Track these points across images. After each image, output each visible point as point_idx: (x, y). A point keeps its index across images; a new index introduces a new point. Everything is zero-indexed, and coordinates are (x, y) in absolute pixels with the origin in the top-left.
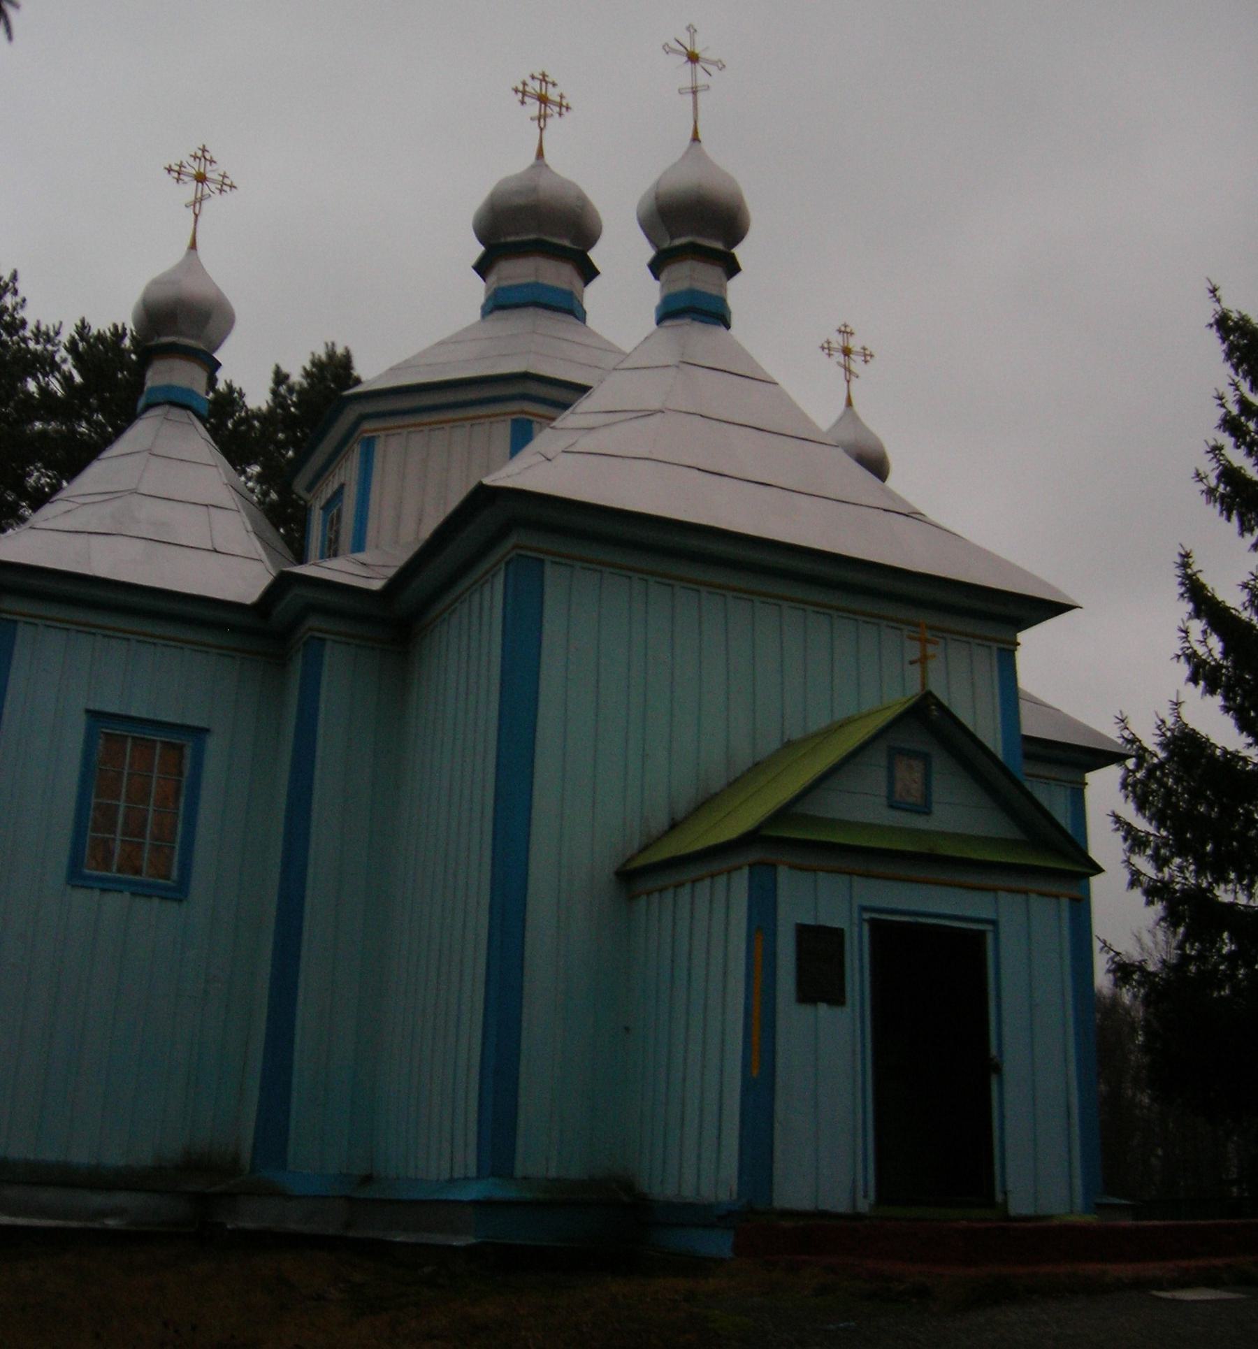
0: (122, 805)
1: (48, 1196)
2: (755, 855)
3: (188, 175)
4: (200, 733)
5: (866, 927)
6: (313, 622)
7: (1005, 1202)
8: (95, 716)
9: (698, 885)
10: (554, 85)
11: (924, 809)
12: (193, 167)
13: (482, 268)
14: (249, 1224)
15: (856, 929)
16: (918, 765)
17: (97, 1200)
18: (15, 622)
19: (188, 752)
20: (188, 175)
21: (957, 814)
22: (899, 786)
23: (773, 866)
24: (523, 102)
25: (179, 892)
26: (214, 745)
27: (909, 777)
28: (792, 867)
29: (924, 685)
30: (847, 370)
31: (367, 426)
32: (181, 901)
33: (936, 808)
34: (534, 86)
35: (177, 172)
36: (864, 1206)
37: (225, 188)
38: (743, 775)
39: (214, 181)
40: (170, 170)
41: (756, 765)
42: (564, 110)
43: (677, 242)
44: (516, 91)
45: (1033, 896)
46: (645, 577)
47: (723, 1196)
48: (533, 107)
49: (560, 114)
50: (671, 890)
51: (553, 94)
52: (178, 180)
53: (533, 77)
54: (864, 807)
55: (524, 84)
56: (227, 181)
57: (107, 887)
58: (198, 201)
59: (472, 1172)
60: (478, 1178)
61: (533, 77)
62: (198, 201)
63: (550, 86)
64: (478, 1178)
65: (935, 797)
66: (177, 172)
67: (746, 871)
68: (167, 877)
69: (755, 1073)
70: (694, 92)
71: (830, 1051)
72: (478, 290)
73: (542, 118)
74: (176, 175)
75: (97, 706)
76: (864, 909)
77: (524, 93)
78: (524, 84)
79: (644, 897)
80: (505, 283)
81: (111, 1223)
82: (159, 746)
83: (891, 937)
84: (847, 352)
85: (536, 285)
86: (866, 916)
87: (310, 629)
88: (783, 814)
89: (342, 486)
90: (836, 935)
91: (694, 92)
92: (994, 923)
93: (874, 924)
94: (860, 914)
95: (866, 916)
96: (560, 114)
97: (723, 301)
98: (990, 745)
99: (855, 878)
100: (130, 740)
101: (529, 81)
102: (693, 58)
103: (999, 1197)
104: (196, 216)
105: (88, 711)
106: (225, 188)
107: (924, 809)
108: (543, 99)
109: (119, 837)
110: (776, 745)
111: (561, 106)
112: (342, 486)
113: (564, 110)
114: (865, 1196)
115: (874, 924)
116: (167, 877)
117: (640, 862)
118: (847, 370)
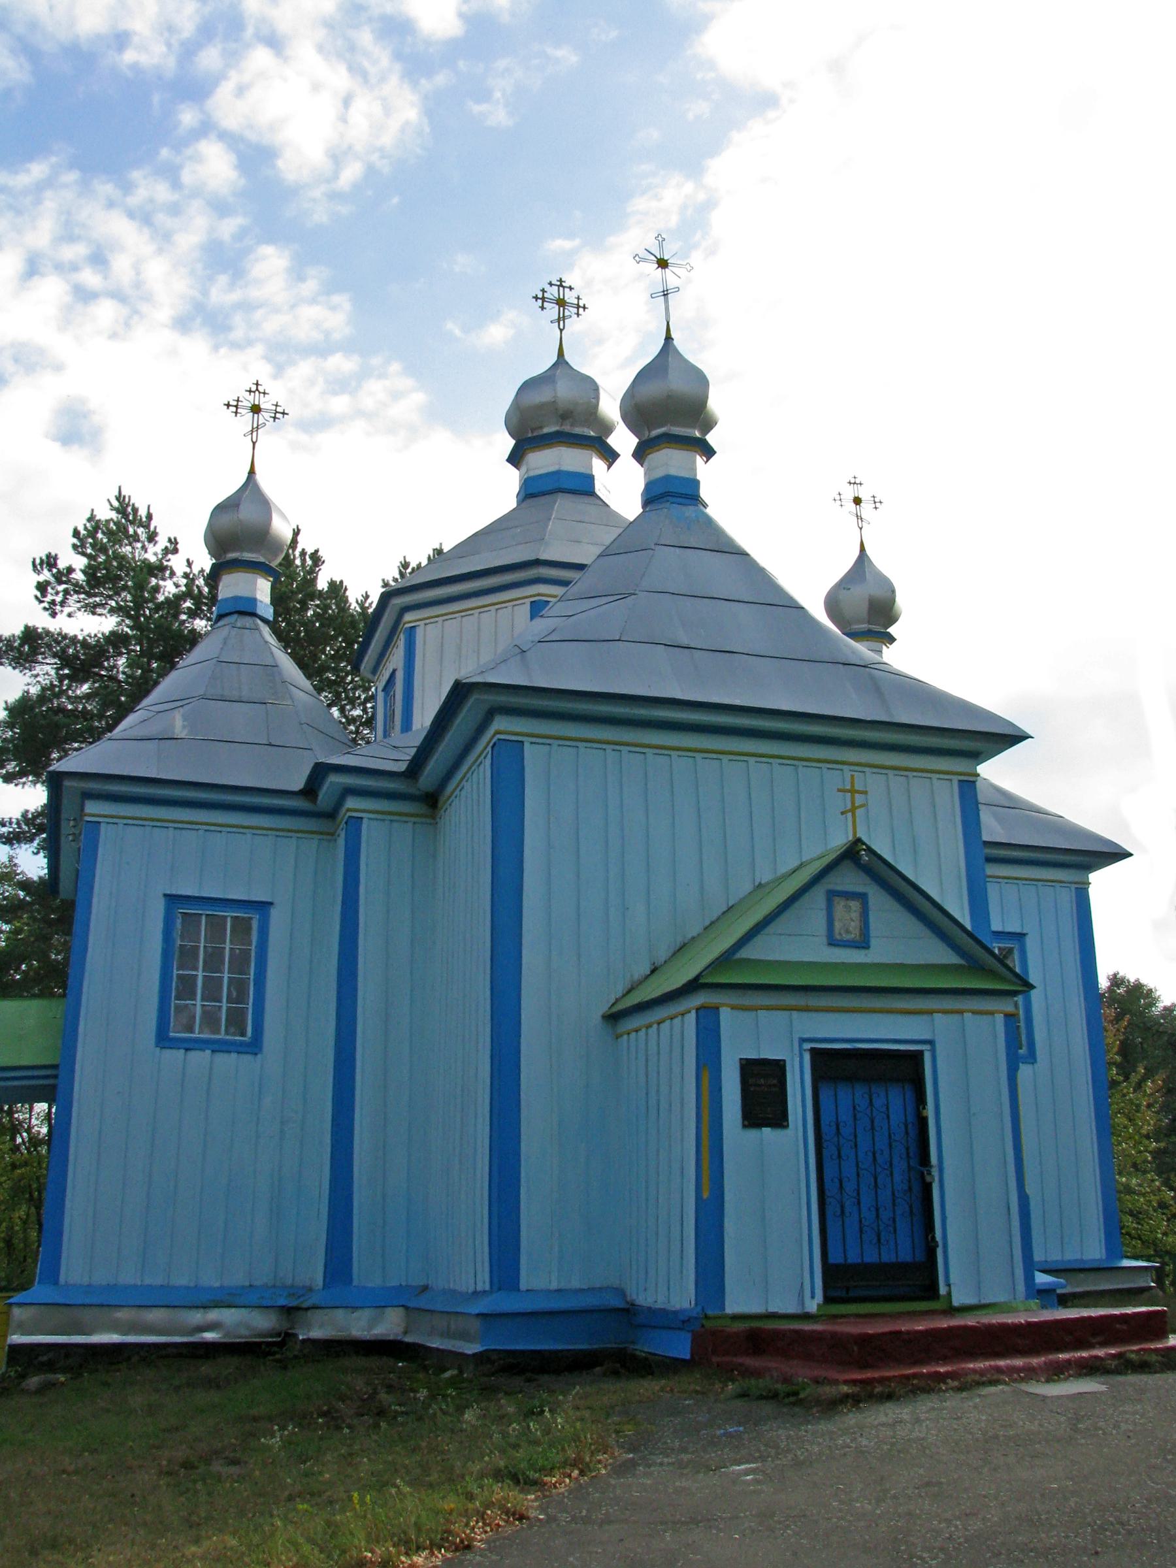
0: (200, 974)
1: (155, 1316)
2: (700, 999)
3: (244, 407)
4: (263, 907)
5: (807, 1057)
6: (351, 803)
7: (949, 1294)
8: (173, 900)
9: (662, 1025)
10: (571, 288)
11: (863, 943)
12: (248, 400)
13: (515, 459)
14: (316, 1333)
15: (797, 1059)
16: (855, 905)
17: (197, 1317)
18: (99, 823)
19: (255, 925)
20: (244, 407)
21: (896, 943)
22: (838, 925)
23: (716, 1009)
24: (542, 308)
25: (254, 1047)
26: (278, 918)
27: (847, 917)
28: (733, 1008)
29: (855, 833)
30: (859, 517)
31: (408, 617)
32: (256, 1054)
33: (873, 942)
34: (553, 292)
35: (234, 406)
36: (812, 1306)
37: (278, 415)
38: (718, 919)
39: (267, 411)
40: (228, 405)
41: (730, 908)
42: (581, 310)
43: (655, 433)
44: (536, 298)
45: (967, 1015)
46: (618, 747)
47: (686, 1305)
48: (553, 311)
49: (578, 315)
50: (644, 1030)
51: (570, 297)
52: (236, 413)
53: (551, 284)
54: (802, 945)
55: (543, 291)
56: (279, 409)
57: (189, 1046)
58: (255, 429)
59: (487, 1287)
60: (491, 1291)
61: (551, 284)
62: (255, 429)
63: (567, 290)
64: (491, 1291)
65: (873, 933)
66: (234, 406)
67: (693, 1013)
68: (243, 1034)
69: (706, 1195)
70: (665, 294)
71: (774, 1173)
72: (512, 479)
73: (561, 319)
74: (234, 409)
75: (168, 892)
76: (803, 1040)
77: (543, 299)
78: (543, 291)
79: (625, 1037)
80: (532, 474)
81: (210, 1336)
82: (229, 920)
83: (834, 1066)
84: (857, 501)
85: (558, 473)
86: (807, 1046)
87: (349, 810)
88: (726, 960)
89: (394, 671)
90: (778, 1068)
91: (665, 294)
92: (930, 1042)
93: (813, 1051)
94: (800, 1046)
95: (807, 1046)
96: (578, 315)
97: (695, 484)
98: (742, 951)
99: (795, 1014)
100: (204, 918)
101: (547, 288)
102: (663, 264)
103: (943, 1290)
104: (254, 443)
105: (165, 895)
106: (278, 415)
107: (863, 943)
108: (561, 303)
109: (199, 1002)
110: (747, 887)
111: (578, 307)
112: (394, 671)
113: (581, 310)
114: (813, 1297)
115: (813, 1051)
116: (243, 1034)
117: (620, 1006)
118: (859, 517)
